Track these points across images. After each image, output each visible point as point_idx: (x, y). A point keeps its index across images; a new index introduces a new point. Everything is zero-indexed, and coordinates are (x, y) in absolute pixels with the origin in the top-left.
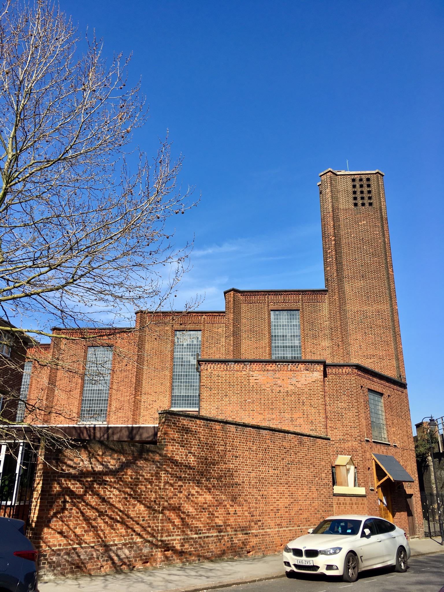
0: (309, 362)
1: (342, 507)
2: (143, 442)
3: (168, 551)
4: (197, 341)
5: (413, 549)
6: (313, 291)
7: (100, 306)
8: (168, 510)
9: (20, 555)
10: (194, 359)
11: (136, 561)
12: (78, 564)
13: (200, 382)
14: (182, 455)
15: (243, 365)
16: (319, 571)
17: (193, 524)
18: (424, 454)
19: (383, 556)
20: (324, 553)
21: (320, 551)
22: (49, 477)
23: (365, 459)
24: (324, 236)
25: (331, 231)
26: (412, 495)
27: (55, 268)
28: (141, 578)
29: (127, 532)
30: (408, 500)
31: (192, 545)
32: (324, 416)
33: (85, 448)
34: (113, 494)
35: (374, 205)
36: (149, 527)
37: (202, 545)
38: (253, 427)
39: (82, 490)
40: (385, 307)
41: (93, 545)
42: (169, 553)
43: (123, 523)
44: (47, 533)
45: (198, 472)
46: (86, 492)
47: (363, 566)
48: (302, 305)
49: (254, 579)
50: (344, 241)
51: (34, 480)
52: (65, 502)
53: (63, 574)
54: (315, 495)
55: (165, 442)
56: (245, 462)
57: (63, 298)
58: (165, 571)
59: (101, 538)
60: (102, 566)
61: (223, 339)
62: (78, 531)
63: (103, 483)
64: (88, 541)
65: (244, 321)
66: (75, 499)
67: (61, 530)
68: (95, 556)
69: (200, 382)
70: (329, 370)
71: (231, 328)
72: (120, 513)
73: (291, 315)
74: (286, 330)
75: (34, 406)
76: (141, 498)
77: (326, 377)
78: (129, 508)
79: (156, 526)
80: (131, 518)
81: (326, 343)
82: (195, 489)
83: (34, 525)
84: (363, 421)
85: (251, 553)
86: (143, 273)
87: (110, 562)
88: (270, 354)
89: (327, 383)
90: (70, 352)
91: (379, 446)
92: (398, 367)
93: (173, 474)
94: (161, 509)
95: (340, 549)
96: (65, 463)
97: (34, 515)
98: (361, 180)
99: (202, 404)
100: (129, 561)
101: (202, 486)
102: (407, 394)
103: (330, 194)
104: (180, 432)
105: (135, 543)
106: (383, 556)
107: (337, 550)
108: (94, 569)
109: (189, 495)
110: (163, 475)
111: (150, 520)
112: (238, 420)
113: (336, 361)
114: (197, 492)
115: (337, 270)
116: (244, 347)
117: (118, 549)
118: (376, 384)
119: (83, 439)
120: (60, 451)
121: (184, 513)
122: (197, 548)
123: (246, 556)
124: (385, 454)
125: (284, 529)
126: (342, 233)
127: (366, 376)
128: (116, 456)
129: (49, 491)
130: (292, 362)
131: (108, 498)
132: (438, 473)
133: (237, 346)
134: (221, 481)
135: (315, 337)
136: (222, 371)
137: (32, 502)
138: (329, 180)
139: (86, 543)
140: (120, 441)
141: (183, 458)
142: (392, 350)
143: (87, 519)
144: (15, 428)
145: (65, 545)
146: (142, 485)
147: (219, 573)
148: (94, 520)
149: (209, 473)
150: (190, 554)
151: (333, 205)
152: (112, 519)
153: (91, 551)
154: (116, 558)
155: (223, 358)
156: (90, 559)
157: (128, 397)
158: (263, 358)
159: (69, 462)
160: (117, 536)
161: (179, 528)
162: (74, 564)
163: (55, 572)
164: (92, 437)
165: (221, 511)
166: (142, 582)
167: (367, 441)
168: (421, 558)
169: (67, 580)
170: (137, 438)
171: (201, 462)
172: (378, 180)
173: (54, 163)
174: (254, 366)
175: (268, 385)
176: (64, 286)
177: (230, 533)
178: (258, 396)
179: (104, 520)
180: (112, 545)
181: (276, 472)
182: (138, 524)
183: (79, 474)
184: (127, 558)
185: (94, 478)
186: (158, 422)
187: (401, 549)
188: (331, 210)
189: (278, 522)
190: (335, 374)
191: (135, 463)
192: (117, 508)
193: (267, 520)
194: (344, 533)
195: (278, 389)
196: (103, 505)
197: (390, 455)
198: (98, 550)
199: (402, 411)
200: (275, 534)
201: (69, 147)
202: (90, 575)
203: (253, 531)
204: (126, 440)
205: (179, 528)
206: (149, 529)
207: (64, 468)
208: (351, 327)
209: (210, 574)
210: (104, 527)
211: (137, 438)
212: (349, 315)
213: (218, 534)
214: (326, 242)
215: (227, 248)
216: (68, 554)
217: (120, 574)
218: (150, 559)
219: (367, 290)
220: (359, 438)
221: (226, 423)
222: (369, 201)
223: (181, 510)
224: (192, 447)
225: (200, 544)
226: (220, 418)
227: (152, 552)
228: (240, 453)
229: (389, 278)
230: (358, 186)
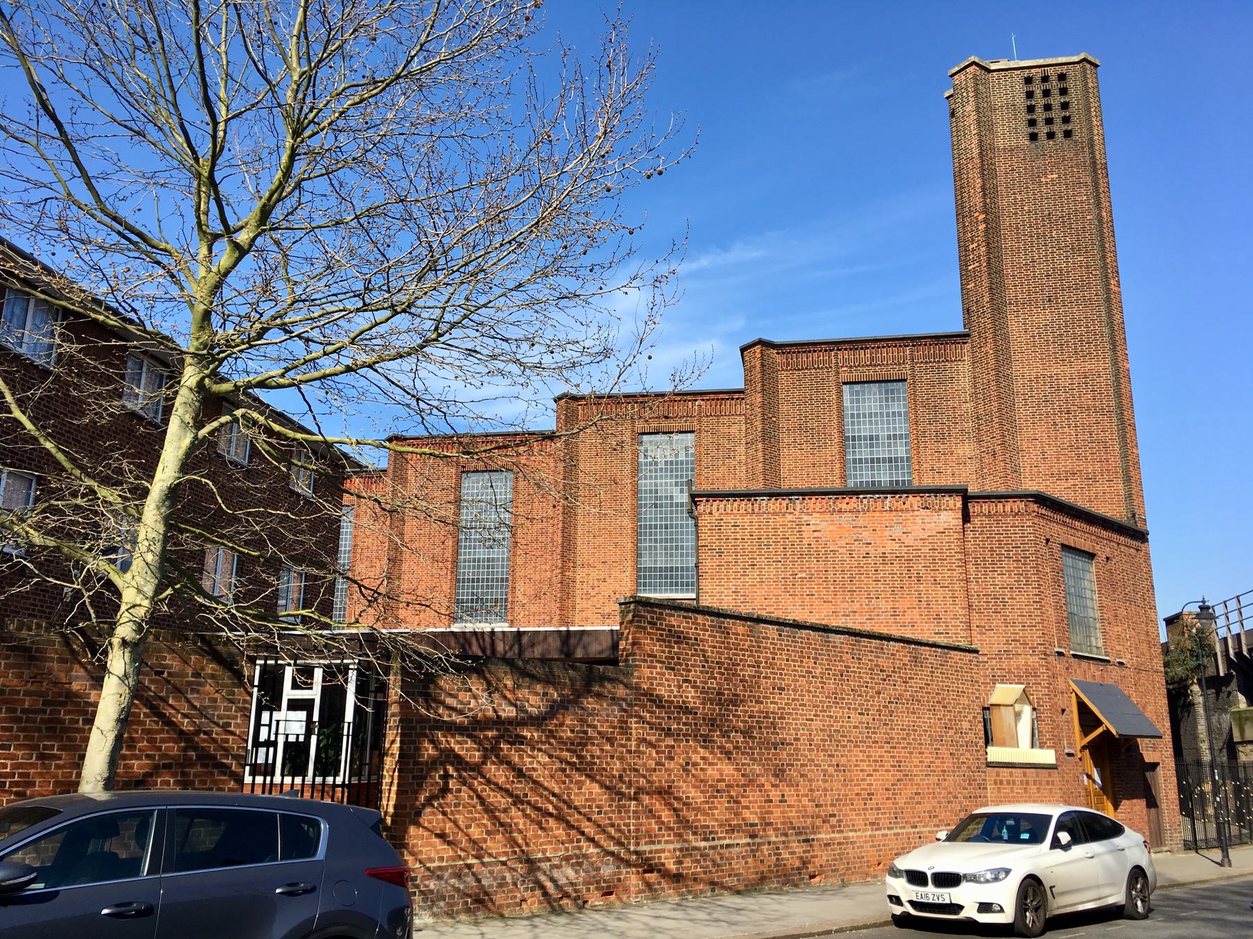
0: (929, 491)
1: (1006, 790)
2: (592, 662)
3: (651, 871)
4: (687, 455)
5: (1161, 874)
6: (937, 337)
7: (498, 387)
8: (648, 793)
9: (377, 875)
10: (682, 491)
11: (588, 890)
12: (476, 894)
13: (698, 539)
14: (669, 686)
15: (787, 501)
16: (963, 915)
17: (699, 821)
18: (1181, 680)
19: (1098, 887)
20: (974, 879)
21: (965, 876)
22: (413, 729)
23: (1053, 692)
24: (961, 213)
25: (977, 200)
26: (1158, 764)
27: (404, 311)
28: (601, 923)
29: (568, 835)
30: (1148, 774)
31: (698, 861)
32: (965, 604)
33: (479, 672)
34: (538, 763)
35: (1077, 136)
36: (613, 825)
37: (718, 861)
38: (814, 628)
39: (477, 753)
40: (1102, 366)
41: (504, 859)
42: (652, 877)
43: (560, 818)
44: (416, 837)
45: (704, 719)
46: (485, 758)
47: (1055, 906)
48: (913, 368)
49: (829, 928)
50: (1006, 222)
51: (384, 735)
52: (446, 776)
53: (450, 915)
54: (948, 764)
55: (634, 660)
56: (801, 699)
57: (422, 373)
58: (646, 911)
59: (519, 846)
60: (524, 900)
61: (742, 449)
62: (475, 832)
63: (519, 740)
64: (494, 852)
65: (784, 408)
66: (465, 770)
67: (443, 830)
68: (509, 879)
69: (698, 539)
70: (974, 508)
71: (758, 424)
72: (554, 799)
73: (887, 393)
74: (876, 423)
75: (375, 592)
76: (592, 770)
77: (969, 522)
78: (570, 788)
79: (625, 825)
80: (576, 808)
81: (967, 449)
82: (698, 753)
83: (389, 820)
84: (1051, 611)
85: (817, 879)
86: (579, 312)
87: (538, 892)
88: (844, 477)
89: (970, 535)
90: (425, 482)
91: (1084, 664)
92: (1129, 496)
93: (654, 724)
94: (632, 791)
95: (1008, 872)
96: (443, 703)
97: (389, 802)
98: (1045, 79)
99: (703, 583)
100: (576, 891)
101: (713, 748)
102: (1147, 554)
103: (973, 117)
104: (664, 641)
105: (585, 856)
106: (1098, 887)
107: (1000, 874)
108: (509, 905)
109: (687, 764)
110: (634, 726)
111: (613, 812)
112: (778, 614)
113: (990, 487)
114: (703, 758)
115: (991, 289)
116: (786, 464)
117: (553, 867)
118: (1079, 534)
119: (476, 657)
120: (431, 679)
121: (678, 799)
122: (707, 867)
123: (808, 885)
124: (1098, 680)
125: (883, 832)
126: (1003, 203)
127: (1058, 517)
128: (539, 688)
129: (413, 756)
130: (894, 492)
131: (528, 769)
132: (1214, 719)
133: (772, 462)
134: (750, 737)
135: (941, 437)
136: (742, 515)
137: (382, 777)
138: (971, 84)
139: (490, 855)
140: (544, 660)
141: (672, 691)
142: (1115, 460)
143: (489, 810)
144: (345, 635)
145: (450, 858)
146: (593, 744)
147: (755, 916)
148: (505, 811)
149: (727, 720)
150: (695, 880)
151: (981, 141)
152: (539, 809)
153: (500, 871)
154: (549, 885)
155: (742, 487)
156: (500, 885)
157: (548, 574)
158: (828, 486)
159: (449, 701)
160: (551, 843)
161: (670, 829)
162: (469, 896)
163: (435, 909)
164: (488, 652)
165: (754, 795)
166: (606, 930)
167: (1060, 654)
168: (1176, 892)
169: (458, 925)
170: (579, 654)
171: (710, 699)
172: (1085, 76)
173: (388, 85)
174: (811, 503)
175: (843, 543)
176: (422, 347)
177: (773, 839)
178: (821, 565)
179: (523, 811)
180: (540, 860)
181: (864, 718)
182: (589, 820)
183: (469, 723)
184: (572, 884)
185: (498, 730)
186: (618, 619)
187: (1138, 873)
188: (976, 151)
189: (872, 818)
190: (989, 516)
191: (577, 703)
192: (546, 789)
193: (847, 815)
194: (1014, 839)
195: (864, 550)
196: (520, 782)
197: (1111, 682)
198: (515, 870)
199: (1140, 590)
200: (866, 842)
201: (418, 48)
202: (502, 916)
203: (820, 836)
204: (556, 656)
205: (670, 829)
206: (612, 830)
207: (441, 711)
208: (1022, 413)
209: (735, 918)
210: (525, 824)
211: (579, 654)
212: (1018, 386)
213: (749, 840)
214: (964, 227)
215: (740, 253)
216: (458, 876)
217: (559, 915)
218: (615, 886)
219: (1060, 328)
220: (1041, 648)
221: (759, 620)
222: (1065, 127)
223: (672, 793)
224: (689, 671)
225: (713, 861)
226: (744, 610)
227: (620, 873)
228: (788, 680)
229: (1111, 301)
230: (1038, 93)
